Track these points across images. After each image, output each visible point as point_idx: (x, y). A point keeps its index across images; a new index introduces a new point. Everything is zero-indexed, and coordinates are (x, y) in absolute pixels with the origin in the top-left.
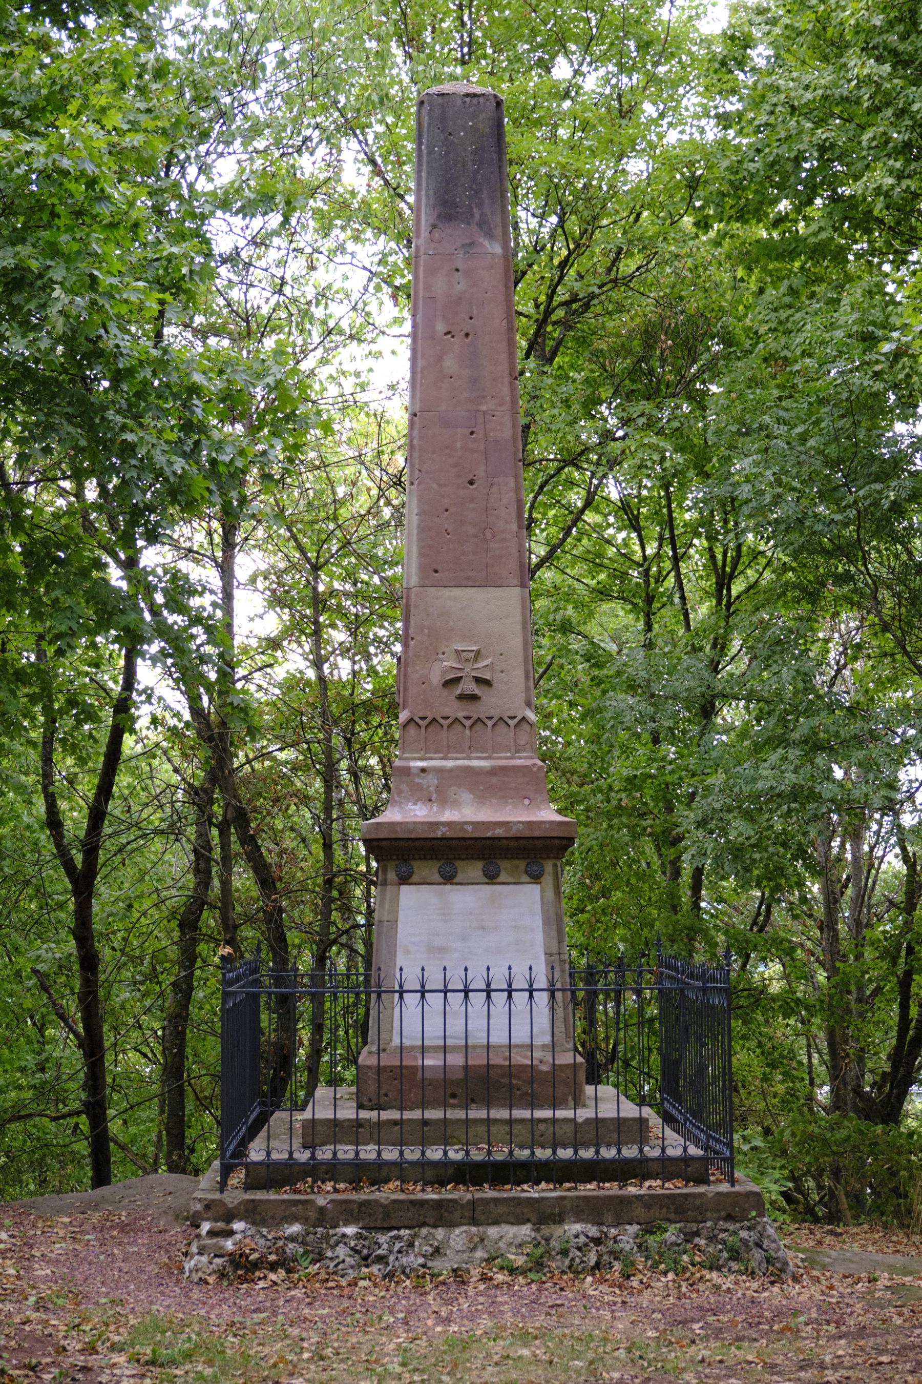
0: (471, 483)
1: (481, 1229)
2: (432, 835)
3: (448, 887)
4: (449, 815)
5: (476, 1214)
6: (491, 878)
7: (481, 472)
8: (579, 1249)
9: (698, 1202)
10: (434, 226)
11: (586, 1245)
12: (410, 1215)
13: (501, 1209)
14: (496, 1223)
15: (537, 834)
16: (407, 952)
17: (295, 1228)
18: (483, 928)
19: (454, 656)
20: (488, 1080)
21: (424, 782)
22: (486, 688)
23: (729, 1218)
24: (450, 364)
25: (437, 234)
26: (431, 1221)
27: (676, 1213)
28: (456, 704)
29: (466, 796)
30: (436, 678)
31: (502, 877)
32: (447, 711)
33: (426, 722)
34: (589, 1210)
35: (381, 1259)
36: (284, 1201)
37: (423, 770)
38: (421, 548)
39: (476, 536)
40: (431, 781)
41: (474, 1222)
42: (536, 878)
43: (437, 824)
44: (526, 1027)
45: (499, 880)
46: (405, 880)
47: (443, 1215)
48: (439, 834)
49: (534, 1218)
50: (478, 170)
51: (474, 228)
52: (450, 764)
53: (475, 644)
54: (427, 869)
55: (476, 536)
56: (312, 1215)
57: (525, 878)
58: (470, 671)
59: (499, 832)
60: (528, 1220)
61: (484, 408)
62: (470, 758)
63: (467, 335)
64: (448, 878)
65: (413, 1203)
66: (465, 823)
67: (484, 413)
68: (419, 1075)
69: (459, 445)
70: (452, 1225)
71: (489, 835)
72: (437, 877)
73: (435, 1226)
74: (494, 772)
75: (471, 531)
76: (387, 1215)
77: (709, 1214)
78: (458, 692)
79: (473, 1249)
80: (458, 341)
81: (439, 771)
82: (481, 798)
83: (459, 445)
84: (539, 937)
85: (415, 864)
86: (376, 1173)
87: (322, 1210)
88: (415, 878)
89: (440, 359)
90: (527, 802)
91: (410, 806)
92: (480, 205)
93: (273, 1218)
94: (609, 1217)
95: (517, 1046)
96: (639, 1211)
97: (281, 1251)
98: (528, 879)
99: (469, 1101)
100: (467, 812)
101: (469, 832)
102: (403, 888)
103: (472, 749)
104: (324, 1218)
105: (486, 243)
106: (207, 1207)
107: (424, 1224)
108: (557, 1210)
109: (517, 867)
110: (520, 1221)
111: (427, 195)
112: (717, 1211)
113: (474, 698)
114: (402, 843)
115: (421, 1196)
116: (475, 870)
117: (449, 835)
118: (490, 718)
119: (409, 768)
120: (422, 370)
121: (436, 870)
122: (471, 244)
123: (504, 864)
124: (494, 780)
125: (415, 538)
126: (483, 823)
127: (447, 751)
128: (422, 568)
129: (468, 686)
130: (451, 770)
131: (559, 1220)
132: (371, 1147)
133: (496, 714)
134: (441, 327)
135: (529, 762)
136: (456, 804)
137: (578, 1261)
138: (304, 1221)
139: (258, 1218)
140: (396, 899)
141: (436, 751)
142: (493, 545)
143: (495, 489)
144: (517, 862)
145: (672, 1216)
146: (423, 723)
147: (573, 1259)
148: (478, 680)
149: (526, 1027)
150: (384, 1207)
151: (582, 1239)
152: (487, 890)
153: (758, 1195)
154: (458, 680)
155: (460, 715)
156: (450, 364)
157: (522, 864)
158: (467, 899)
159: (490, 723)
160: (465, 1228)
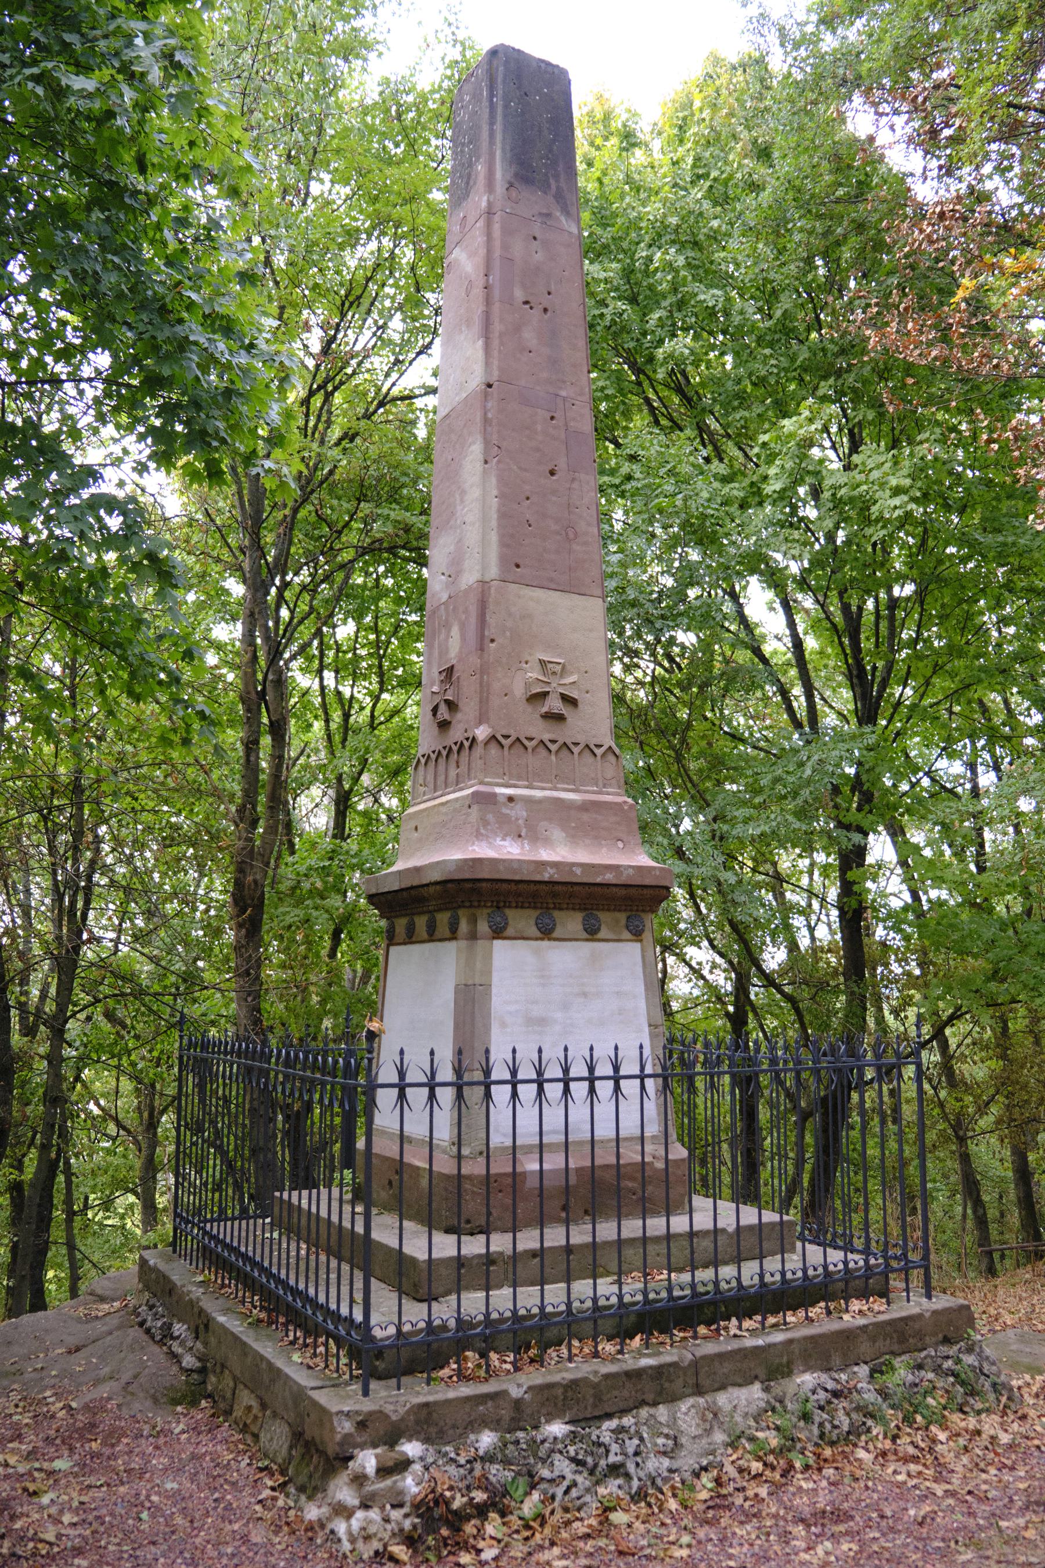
0: (552, 473)
1: (709, 1398)
2: (538, 878)
3: (546, 943)
4: (545, 855)
5: (702, 1378)
6: (592, 933)
7: (562, 464)
8: (821, 1408)
9: (917, 1326)
10: (511, 185)
11: (829, 1402)
12: (626, 1393)
13: (727, 1367)
14: (723, 1387)
15: (647, 882)
16: (503, 1025)
17: (487, 1439)
18: (585, 995)
19: (538, 667)
20: (602, 1187)
21: (513, 813)
22: (570, 708)
23: (947, 1341)
24: (529, 336)
25: (514, 193)
26: (650, 1397)
27: (900, 1342)
28: (541, 723)
29: (557, 834)
30: (519, 691)
31: (602, 935)
32: (532, 732)
33: (509, 741)
34: (820, 1352)
35: (616, 1470)
36: (467, 1399)
37: (511, 799)
38: (502, 536)
39: (558, 533)
40: (518, 812)
41: (699, 1391)
42: (637, 934)
43: (544, 864)
44: (631, 1119)
45: (601, 935)
46: (498, 933)
47: (659, 1386)
48: (546, 877)
49: (762, 1373)
50: (554, 141)
51: (550, 199)
52: (538, 794)
53: (559, 656)
54: (521, 920)
55: (558, 533)
56: (506, 1414)
57: (627, 935)
58: (557, 687)
59: (609, 877)
60: (756, 1377)
61: (564, 393)
62: (556, 789)
63: (545, 310)
64: (546, 932)
65: (629, 1375)
66: (574, 864)
67: (564, 399)
68: (424, 1182)
69: (539, 428)
70: (673, 1399)
71: (599, 880)
72: (534, 931)
73: (655, 1404)
74: (586, 807)
75: (554, 527)
76: (598, 1398)
77: (927, 1340)
78: (545, 709)
79: (708, 1432)
80: (537, 312)
81: (529, 801)
82: (576, 834)
83: (539, 428)
84: (642, 1005)
85: (510, 913)
86: (530, 1336)
87: (518, 1403)
88: (510, 931)
89: (518, 329)
90: (620, 845)
91: (499, 842)
92: (557, 177)
93: (454, 1427)
94: (837, 1360)
95: (626, 1139)
96: (865, 1348)
97: (484, 1483)
98: (629, 936)
99: (593, 1212)
100: (560, 852)
101: (579, 876)
102: (498, 944)
103: (557, 779)
104: (518, 1417)
105: (563, 219)
106: (362, 1425)
107: (643, 1403)
108: (785, 1360)
109: (617, 921)
110: (747, 1381)
111: (503, 150)
112: (936, 1334)
113: (560, 718)
114: (505, 886)
115: (629, 1363)
116: (571, 922)
117: (557, 877)
118: (576, 744)
119: (495, 795)
120: (501, 335)
121: (532, 922)
122: (548, 215)
123: (603, 916)
124: (585, 817)
125: (494, 523)
126: (593, 866)
127: (530, 779)
128: (503, 560)
129: (554, 704)
130: (540, 801)
131: (784, 1371)
132: (507, 1291)
133: (582, 739)
134: (519, 295)
135: (619, 799)
136: (547, 842)
137: (828, 1426)
138: (494, 1424)
139: (433, 1430)
140: (488, 958)
141: (519, 778)
142: (576, 547)
143: (575, 485)
144: (618, 915)
145: (896, 1348)
146: (506, 743)
147: (821, 1425)
148: (566, 699)
149: (631, 1119)
150: (595, 1386)
151: (822, 1395)
152: (586, 948)
153: (968, 1307)
154: (545, 694)
155: (546, 737)
156: (529, 336)
157: (622, 917)
158: (566, 958)
159: (576, 750)
160: (691, 1401)
